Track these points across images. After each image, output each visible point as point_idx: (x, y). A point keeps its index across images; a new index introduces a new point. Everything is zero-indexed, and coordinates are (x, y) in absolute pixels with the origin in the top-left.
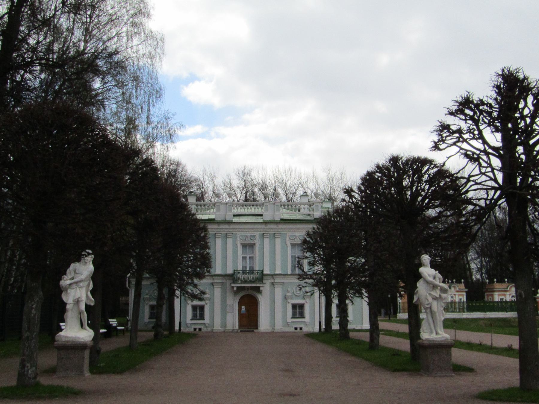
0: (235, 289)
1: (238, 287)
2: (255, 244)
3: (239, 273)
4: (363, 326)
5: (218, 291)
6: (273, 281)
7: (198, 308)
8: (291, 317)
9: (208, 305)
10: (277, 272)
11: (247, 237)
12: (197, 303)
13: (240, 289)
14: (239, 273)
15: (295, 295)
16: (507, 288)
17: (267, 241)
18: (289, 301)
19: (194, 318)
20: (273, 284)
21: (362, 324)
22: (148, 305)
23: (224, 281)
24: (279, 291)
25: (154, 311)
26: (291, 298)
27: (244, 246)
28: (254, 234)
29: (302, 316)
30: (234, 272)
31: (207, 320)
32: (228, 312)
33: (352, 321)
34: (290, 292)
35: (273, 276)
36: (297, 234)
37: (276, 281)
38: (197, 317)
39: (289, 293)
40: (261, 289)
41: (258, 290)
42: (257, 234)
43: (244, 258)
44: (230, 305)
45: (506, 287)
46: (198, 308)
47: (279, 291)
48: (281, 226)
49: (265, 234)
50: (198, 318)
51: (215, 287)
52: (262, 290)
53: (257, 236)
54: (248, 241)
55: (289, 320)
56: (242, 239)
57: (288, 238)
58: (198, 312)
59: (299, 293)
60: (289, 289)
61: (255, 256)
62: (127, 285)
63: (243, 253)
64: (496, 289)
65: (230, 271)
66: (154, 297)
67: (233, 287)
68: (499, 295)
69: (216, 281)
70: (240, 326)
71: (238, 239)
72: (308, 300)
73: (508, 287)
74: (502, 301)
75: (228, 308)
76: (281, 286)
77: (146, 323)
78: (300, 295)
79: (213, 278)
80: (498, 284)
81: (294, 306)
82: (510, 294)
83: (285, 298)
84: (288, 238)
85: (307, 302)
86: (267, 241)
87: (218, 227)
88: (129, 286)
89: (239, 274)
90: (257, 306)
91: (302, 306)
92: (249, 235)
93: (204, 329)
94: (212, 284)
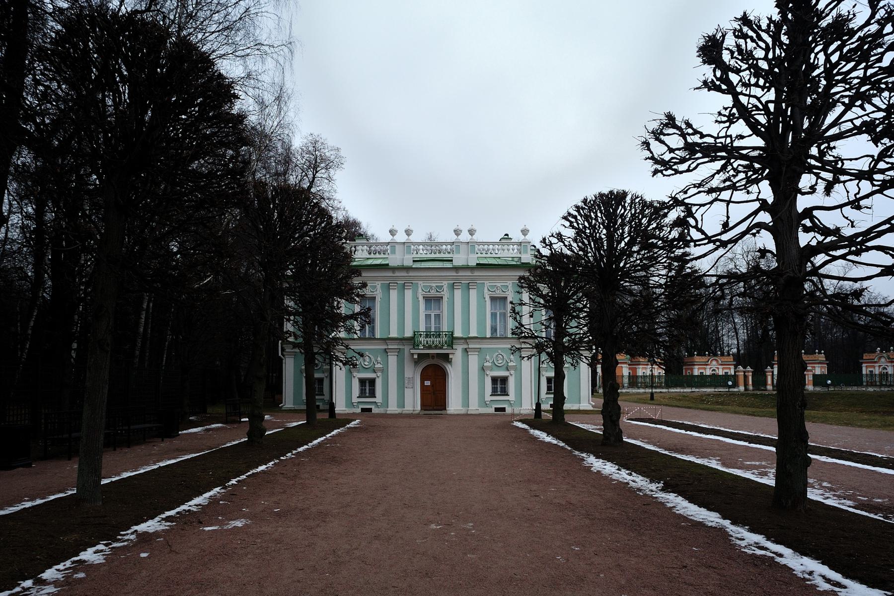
0: (416, 357)
3: (421, 335)
5: (393, 360)
6: (466, 346)
10: (471, 335)
11: (431, 287)
14: (421, 335)
16: (708, 362)
18: (488, 372)
19: (362, 394)
23: (401, 347)
24: (474, 360)
28: (375, 284)
29: (505, 392)
30: (415, 335)
31: (379, 398)
35: (466, 339)
36: (499, 285)
37: (470, 346)
41: (446, 358)
42: (445, 284)
44: (409, 378)
47: (474, 360)
49: (406, 284)
50: (367, 395)
52: (452, 359)
54: (433, 293)
55: (488, 398)
57: (486, 289)
60: (488, 357)
63: (426, 309)
65: (408, 334)
67: (413, 354)
68: (723, 369)
69: (390, 347)
70: (423, 405)
72: (379, 374)
74: (702, 376)
75: (406, 382)
80: (698, 357)
82: (880, 366)
85: (511, 375)
86: (458, 294)
88: (282, 354)
91: (504, 380)
93: (375, 410)
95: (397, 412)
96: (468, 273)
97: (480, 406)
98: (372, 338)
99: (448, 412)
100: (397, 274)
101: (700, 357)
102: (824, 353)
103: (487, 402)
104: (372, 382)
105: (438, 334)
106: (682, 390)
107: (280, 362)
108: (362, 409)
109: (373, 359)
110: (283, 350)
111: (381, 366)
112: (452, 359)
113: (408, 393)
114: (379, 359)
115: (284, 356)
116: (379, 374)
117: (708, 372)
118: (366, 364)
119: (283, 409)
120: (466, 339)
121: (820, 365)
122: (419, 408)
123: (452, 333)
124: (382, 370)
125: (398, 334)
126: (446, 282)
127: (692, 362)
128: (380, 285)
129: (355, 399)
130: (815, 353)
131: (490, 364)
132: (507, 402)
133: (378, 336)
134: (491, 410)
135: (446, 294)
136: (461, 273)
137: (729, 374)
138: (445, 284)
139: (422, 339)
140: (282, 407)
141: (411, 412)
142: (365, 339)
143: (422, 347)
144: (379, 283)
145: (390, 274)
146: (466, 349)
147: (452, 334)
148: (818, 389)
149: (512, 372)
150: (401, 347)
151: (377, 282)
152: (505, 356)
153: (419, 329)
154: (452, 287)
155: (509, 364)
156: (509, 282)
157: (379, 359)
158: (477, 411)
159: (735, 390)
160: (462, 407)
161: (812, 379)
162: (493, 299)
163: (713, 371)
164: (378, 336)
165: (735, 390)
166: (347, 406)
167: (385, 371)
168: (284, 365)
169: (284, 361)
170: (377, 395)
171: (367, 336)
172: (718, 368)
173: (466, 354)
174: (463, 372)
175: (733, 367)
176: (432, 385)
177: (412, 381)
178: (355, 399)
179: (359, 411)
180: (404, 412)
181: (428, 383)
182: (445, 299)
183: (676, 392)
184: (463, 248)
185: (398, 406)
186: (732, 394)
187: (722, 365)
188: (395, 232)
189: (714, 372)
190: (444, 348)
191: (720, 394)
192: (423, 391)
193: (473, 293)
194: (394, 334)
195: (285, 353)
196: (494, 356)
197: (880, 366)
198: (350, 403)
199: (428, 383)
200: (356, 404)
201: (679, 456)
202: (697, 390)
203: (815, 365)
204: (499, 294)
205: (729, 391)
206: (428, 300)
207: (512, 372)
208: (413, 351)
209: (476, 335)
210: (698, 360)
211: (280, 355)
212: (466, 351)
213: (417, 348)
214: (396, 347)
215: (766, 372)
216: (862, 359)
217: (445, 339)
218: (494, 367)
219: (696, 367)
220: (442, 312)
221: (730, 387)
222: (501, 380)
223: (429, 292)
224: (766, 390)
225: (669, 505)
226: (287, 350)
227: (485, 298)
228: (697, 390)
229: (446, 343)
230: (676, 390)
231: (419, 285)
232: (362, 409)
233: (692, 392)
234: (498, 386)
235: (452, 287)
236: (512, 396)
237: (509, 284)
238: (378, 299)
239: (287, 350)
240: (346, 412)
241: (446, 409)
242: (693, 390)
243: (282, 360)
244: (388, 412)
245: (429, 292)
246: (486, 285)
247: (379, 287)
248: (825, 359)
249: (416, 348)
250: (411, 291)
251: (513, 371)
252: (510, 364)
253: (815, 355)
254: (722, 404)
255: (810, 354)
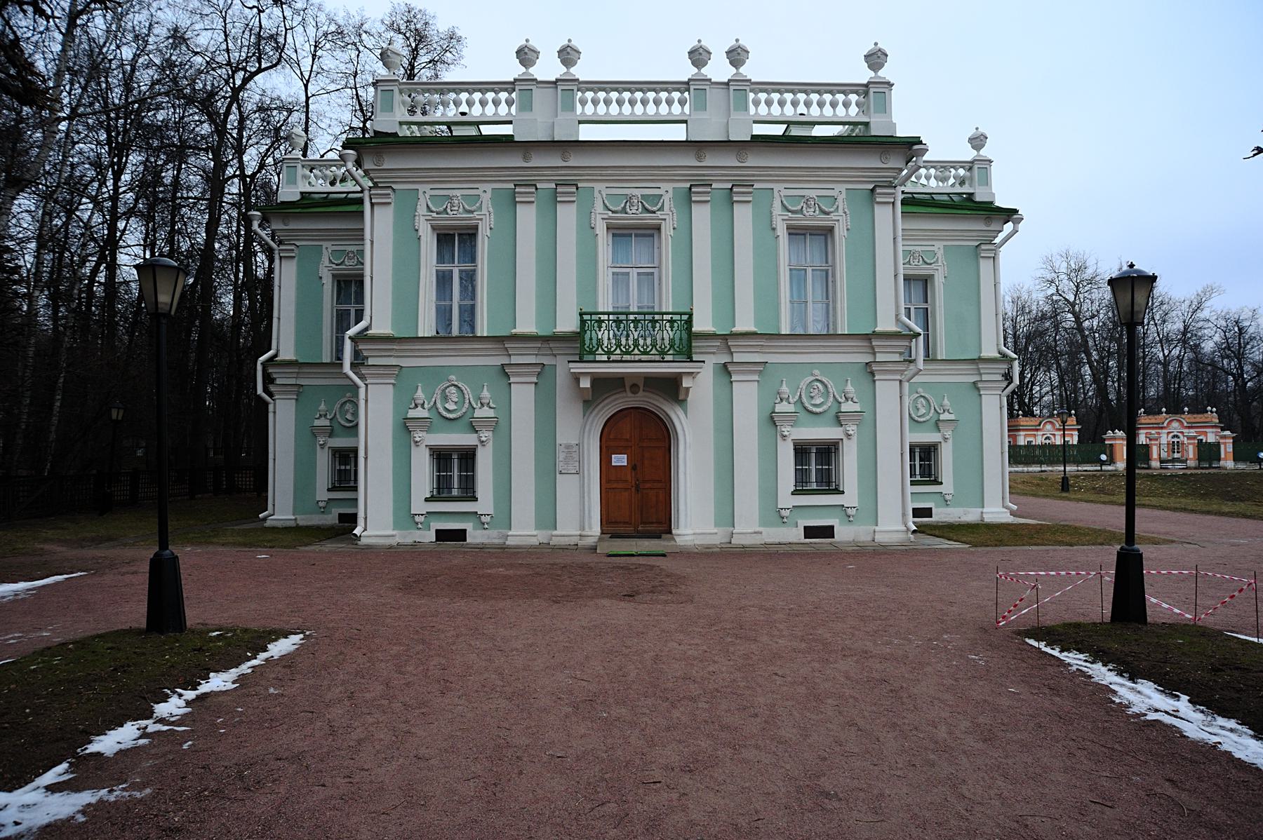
0: (585, 383)
1: (597, 381)
2: (658, 228)
3: (600, 322)
4: (985, 510)
5: (523, 396)
6: (724, 359)
7: (455, 456)
8: (793, 488)
9: (950, 441)
10: (739, 328)
11: (629, 199)
12: (341, 442)
13: (604, 386)
14: (600, 322)
15: (805, 408)
16: (1040, 425)
17: (702, 216)
18: (786, 430)
19: (441, 491)
20: (725, 369)
21: (983, 507)
22: (326, 449)
23: (546, 360)
24: (747, 396)
25: (348, 467)
26: (793, 419)
27: (445, 238)
29: (829, 484)
30: (583, 322)
31: (485, 502)
32: (561, 473)
33: (488, 519)
34: (788, 399)
35: (727, 339)
37: (737, 358)
38: (450, 489)
39: (785, 403)
40: (686, 383)
41: (672, 388)
43: (443, 280)
44: (568, 447)
45: (1037, 424)
46: (455, 456)
47: (747, 396)
48: (753, 160)
50: (455, 492)
51: (512, 380)
52: (688, 389)
53: (666, 199)
54: (635, 215)
55: (786, 499)
56: (613, 209)
57: (777, 204)
58: (456, 473)
59: (453, 411)
60: (785, 388)
61: (660, 273)
62: (260, 390)
64: (1023, 426)
65: (567, 323)
66: (343, 423)
67: (576, 378)
68: (1026, 436)
69: (514, 360)
70: (606, 521)
71: (599, 207)
72: (485, 435)
73: (1040, 423)
74: (1029, 446)
75: (561, 456)
76: (756, 378)
77: (321, 504)
78: (464, 413)
79: (506, 349)
80: (1024, 419)
81: (441, 457)
82: (1169, 433)
83: (772, 420)
84: (777, 204)
85: (848, 436)
86: (702, 216)
87: (521, 163)
88: (266, 390)
89: (600, 327)
90: (652, 378)
91: (827, 452)
92: (638, 192)
93: (475, 536)
94: (504, 371)
95: (534, 541)
96: (730, 160)
97: (764, 522)
98: (470, 337)
99: (680, 541)
100: (537, 161)
101: (1027, 419)
102: (1216, 412)
103: (784, 513)
104: (468, 457)
105: (650, 319)
106: (1026, 469)
107: (261, 411)
108: (438, 531)
109: (469, 394)
110: (268, 380)
111: (491, 413)
112: (688, 389)
113: (566, 487)
114: (486, 394)
115: (271, 395)
116: (485, 435)
117: (1039, 440)
118: (451, 406)
119: (268, 524)
120: (725, 337)
121: (1214, 430)
122: (595, 529)
123: (691, 315)
124: (494, 425)
125: (538, 324)
126: (669, 187)
127: (1017, 426)
128: (489, 194)
129: (419, 506)
130: (1207, 412)
131: (791, 408)
132: (840, 508)
133: (483, 329)
134: (796, 535)
135: (669, 220)
136: (711, 160)
137: (1070, 443)
138: (667, 191)
139: (604, 335)
140: (265, 519)
141: (573, 541)
142: (449, 339)
143: (605, 358)
144: (489, 187)
145: (514, 161)
146: (725, 365)
147: (689, 322)
148: (1241, 466)
149: (852, 429)
150: (546, 360)
151: (482, 187)
152: (830, 384)
153: (596, 303)
154: (687, 198)
155: (844, 408)
156: (663, 185)
157: (486, 394)
158: (758, 537)
159: (1110, 468)
160: (716, 525)
161: (1231, 450)
162: (796, 232)
163: (1174, 437)
164: (483, 329)
165: (1110, 468)
166: (396, 526)
167: (501, 426)
168: (271, 416)
169: (271, 408)
170: (479, 495)
171: (455, 331)
172: (1054, 435)
173: (725, 379)
174: (716, 430)
175: (1076, 433)
176: (633, 466)
177: (575, 456)
178: (419, 506)
179: (431, 536)
180: (554, 541)
181: (620, 460)
182: (667, 230)
183: (1017, 472)
184: (713, 96)
185: (540, 525)
186: (1114, 475)
187: (1189, 428)
188: (531, 55)
189: (1047, 441)
190: (668, 358)
191: (1094, 475)
192: (609, 481)
193: (744, 216)
194: (527, 325)
195: (272, 388)
196: (803, 385)
197: (1169, 433)
198: (405, 517)
199: (620, 460)
200: (421, 519)
201: (1239, 636)
202: (1050, 468)
203: (1207, 430)
204: (812, 218)
205: (1101, 471)
206: (619, 232)
207: (852, 429)
208: (578, 368)
209: (752, 329)
210: (1025, 423)
211: (260, 390)
212: (725, 370)
213: (591, 357)
214: (532, 360)
215: (1105, 440)
216: (1078, 430)
217: (668, 334)
218: (803, 414)
219: (1022, 433)
220: (659, 267)
221: (1102, 463)
222: (819, 452)
223: (624, 211)
224: (1149, 468)
225: (1135, 709)
226: (278, 381)
227: (774, 229)
228: (1050, 468)
229: (672, 346)
230: (1016, 469)
231: (596, 194)
232: (438, 531)
233: (1042, 471)
234: (813, 467)
235: (687, 198)
236: (851, 496)
237: (485, 192)
238: (840, 232)
239: (278, 381)
240: (393, 542)
241: (670, 532)
242: (1043, 469)
243: (267, 404)
244: (510, 542)
245: (624, 211)
246: (421, 195)
247: (486, 198)
248: (1217, 421)
249: (586, 358)
250: (574, 207)
251: (855, 427)
252: (846, 407)
253: (1206, 415)
254: (1101, 491)
255: (1198, 413)
